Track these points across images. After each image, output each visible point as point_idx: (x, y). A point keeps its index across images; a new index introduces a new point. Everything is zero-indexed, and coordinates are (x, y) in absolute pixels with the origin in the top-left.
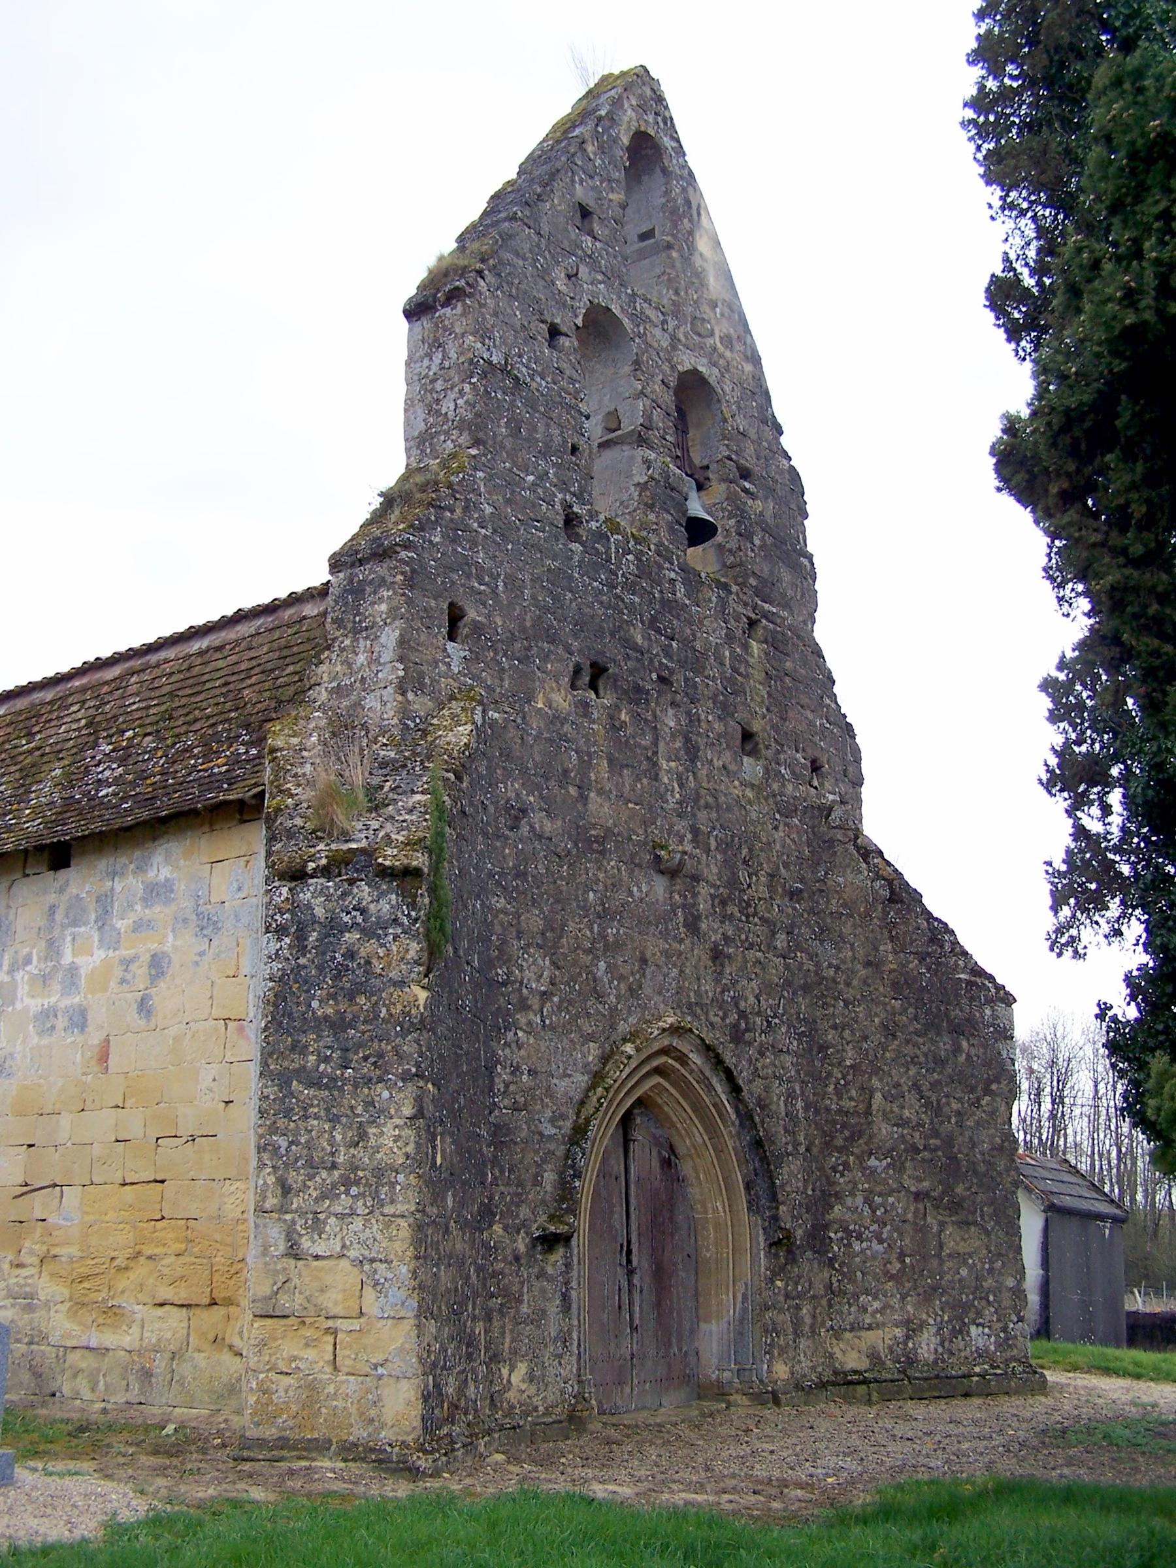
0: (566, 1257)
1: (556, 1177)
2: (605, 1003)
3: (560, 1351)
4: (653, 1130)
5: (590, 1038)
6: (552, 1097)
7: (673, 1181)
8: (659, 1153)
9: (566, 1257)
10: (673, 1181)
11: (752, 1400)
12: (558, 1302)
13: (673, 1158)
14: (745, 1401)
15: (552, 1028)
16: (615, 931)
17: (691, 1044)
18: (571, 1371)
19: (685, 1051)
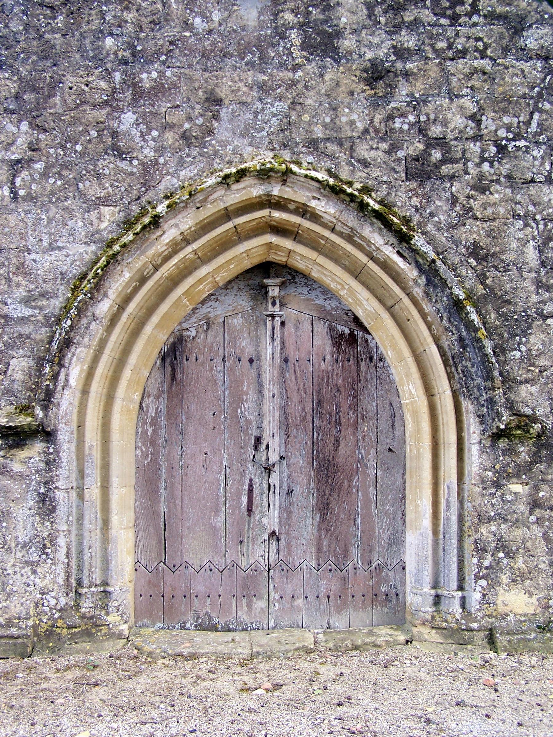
0: (48, 454)
1: (32, 363)
2: (132, 159)
3: (35, 557)
4: (320, 302)
5: (105, 201)
6: (26, 274)
7: (358, 362)
8: (331, 329)
9: (48, 454)
10: (358, 362)
11: (446, 637)
12: (31, 503)
13: (359, 333)
14: (434, 636)
15: (30, 198)
16: (154, 75)
17: (310, 190)
18: (54, 581)
19: (302, 200)
